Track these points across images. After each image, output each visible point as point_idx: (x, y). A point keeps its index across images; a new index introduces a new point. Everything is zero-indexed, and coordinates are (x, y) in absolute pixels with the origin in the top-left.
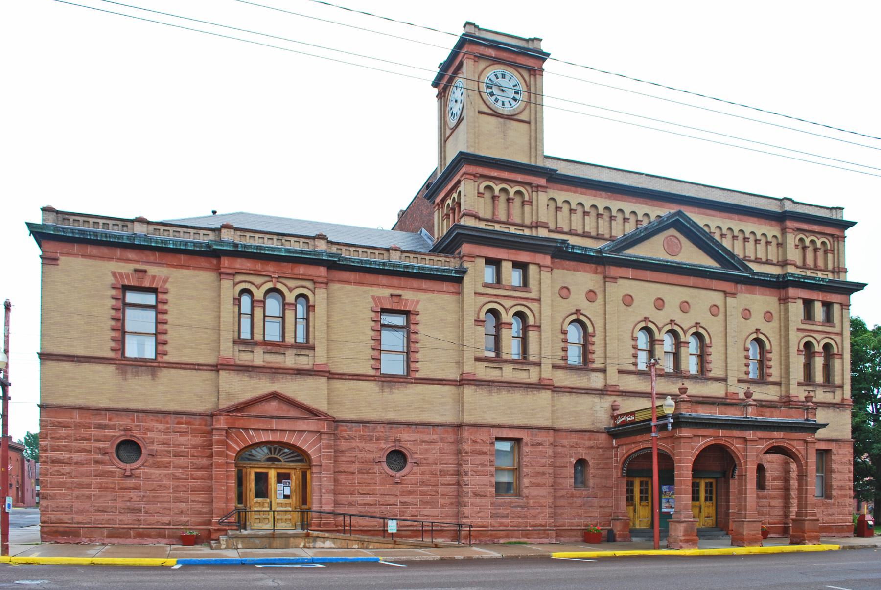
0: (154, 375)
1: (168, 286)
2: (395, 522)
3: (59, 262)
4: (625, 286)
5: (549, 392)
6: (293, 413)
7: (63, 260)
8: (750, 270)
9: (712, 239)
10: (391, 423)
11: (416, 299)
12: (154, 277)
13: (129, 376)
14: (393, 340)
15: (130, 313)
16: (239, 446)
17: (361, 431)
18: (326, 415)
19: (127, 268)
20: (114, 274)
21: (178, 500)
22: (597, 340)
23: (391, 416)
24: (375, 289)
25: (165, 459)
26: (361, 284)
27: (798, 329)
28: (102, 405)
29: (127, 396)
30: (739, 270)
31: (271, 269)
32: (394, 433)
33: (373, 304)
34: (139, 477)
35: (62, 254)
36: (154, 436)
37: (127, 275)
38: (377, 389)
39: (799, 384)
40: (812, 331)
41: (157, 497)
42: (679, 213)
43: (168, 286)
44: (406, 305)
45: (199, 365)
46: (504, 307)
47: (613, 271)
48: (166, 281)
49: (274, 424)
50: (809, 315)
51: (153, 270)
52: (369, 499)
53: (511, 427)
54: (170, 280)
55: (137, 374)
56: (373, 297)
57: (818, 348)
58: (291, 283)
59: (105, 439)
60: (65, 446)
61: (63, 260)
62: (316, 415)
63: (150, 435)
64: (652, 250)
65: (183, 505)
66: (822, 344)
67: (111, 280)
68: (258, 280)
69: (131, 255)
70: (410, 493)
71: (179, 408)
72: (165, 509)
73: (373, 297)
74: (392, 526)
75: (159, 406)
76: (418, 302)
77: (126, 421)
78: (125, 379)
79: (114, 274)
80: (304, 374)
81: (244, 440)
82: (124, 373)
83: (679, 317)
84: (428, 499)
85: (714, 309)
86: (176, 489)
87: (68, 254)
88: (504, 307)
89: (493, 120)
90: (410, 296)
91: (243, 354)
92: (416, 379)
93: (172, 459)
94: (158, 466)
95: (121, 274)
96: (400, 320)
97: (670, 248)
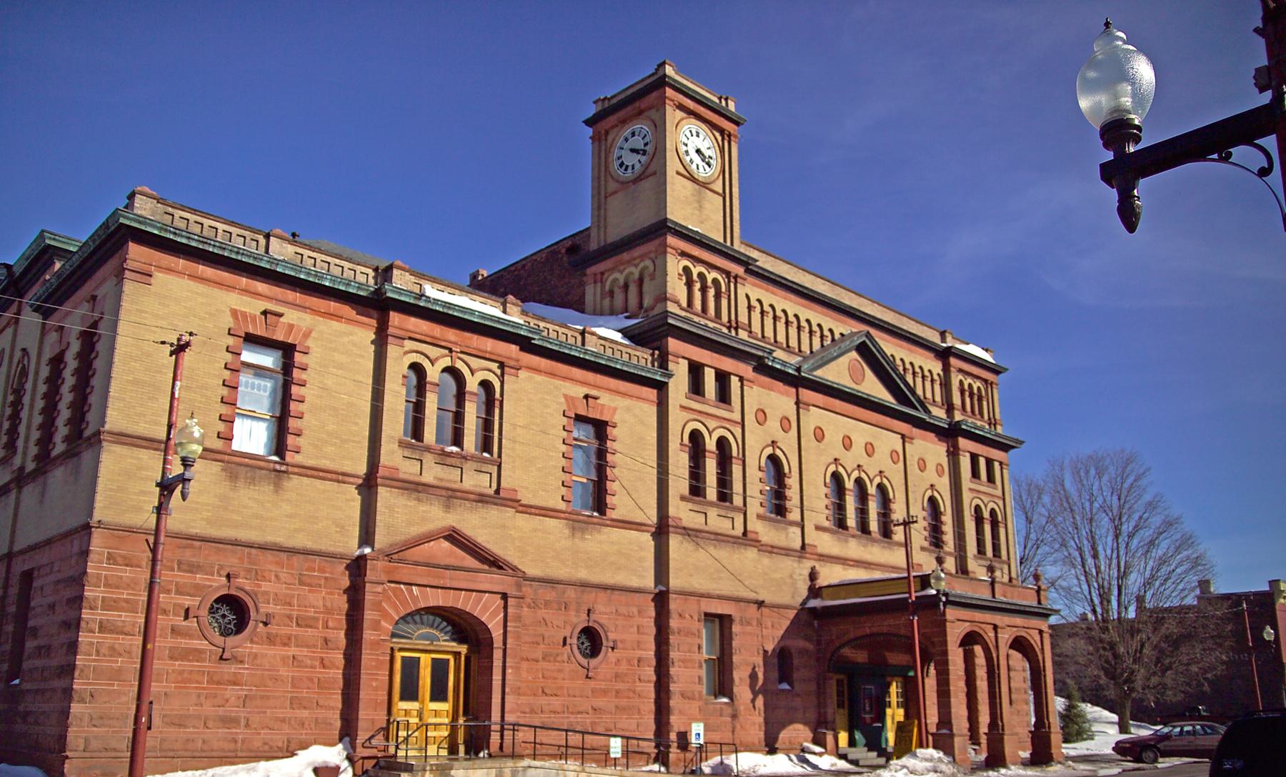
0: (278, 487)
1: (310, 343)
2: (619, 740)
3: (152, 280)
4: (814, 417)
5: (755, 550)
6: (471, 562)
7: (159, 277)
8: (927, 411)
9: (895, 369)
10: (585, 585)
11: (613, 405)
12: (291, 327)
13: (240, 484)
14: (257, 395)
15: (245, 378)
16: (398, 613)
17: (548, 594)
18: (514, 569)
19: (254, 307)
20: (234, 313)
21: (295, 703)
22: (792, 481)
23: (583, 574)
24: (568, 384)
25: (285, 631)
26: (552, 375)
27: (682, 407)
28: (194, 531)
29: (235, 517)
30: (915, 408)
31: (453, 338)
32: (589, 597)
33: (565, 407)
34: (242, 662)
35: (159, 267)
36: (269, 591)
37: (254, 318)
38: (567, 532)
39: (683, 498)
40: (700, 412)
41: (268, 698)
42: (868, 335)
43: (310, 343)
44: (601, 413)
45: (344, 474)
46: (427, 357)
47: (806, 394)
48: (307, 335)
49: (448, 578)
50: (696, 388)
51: (605, 399)
52: (556, 703)
53: (720, 597)
54: (313, 334)
55: (252, 481)
56: (566, 396)
57: (711, 444)
58: (475, 363)
59: (197, 589)
60: (127, 601)
61: (159, 277)
62: (501, 568)
63: (265, 586)
64: (839, 372)
65: (305, 714)
66: (715, 436)
67: (228, 322)
68: (433, 352)
69: (261, 287)
70: (605, 692)
71: (310, 545)
72: (277, 719)
73: (566, 396)
74: (616, 746)
75: (280, 539)
76: (615, 409)
77: (232, 560)
78: (234, 489)
79: (234, 313)
80: (487, 502)
81: (404, 603)
82: (233, 477)
83: (864, 460)
84: (623, 702)
85: (761, 415)
86: (295, 683)
87: (170, 270)
88: (427, 357)
89: (689, 184)
90: (297, 318)
91: (408, 462)
92: (613, 520)
93: (294, 630)
94: (271, 640)
95: (244, 315)
96: (268, 360)
97: (857, 377)
